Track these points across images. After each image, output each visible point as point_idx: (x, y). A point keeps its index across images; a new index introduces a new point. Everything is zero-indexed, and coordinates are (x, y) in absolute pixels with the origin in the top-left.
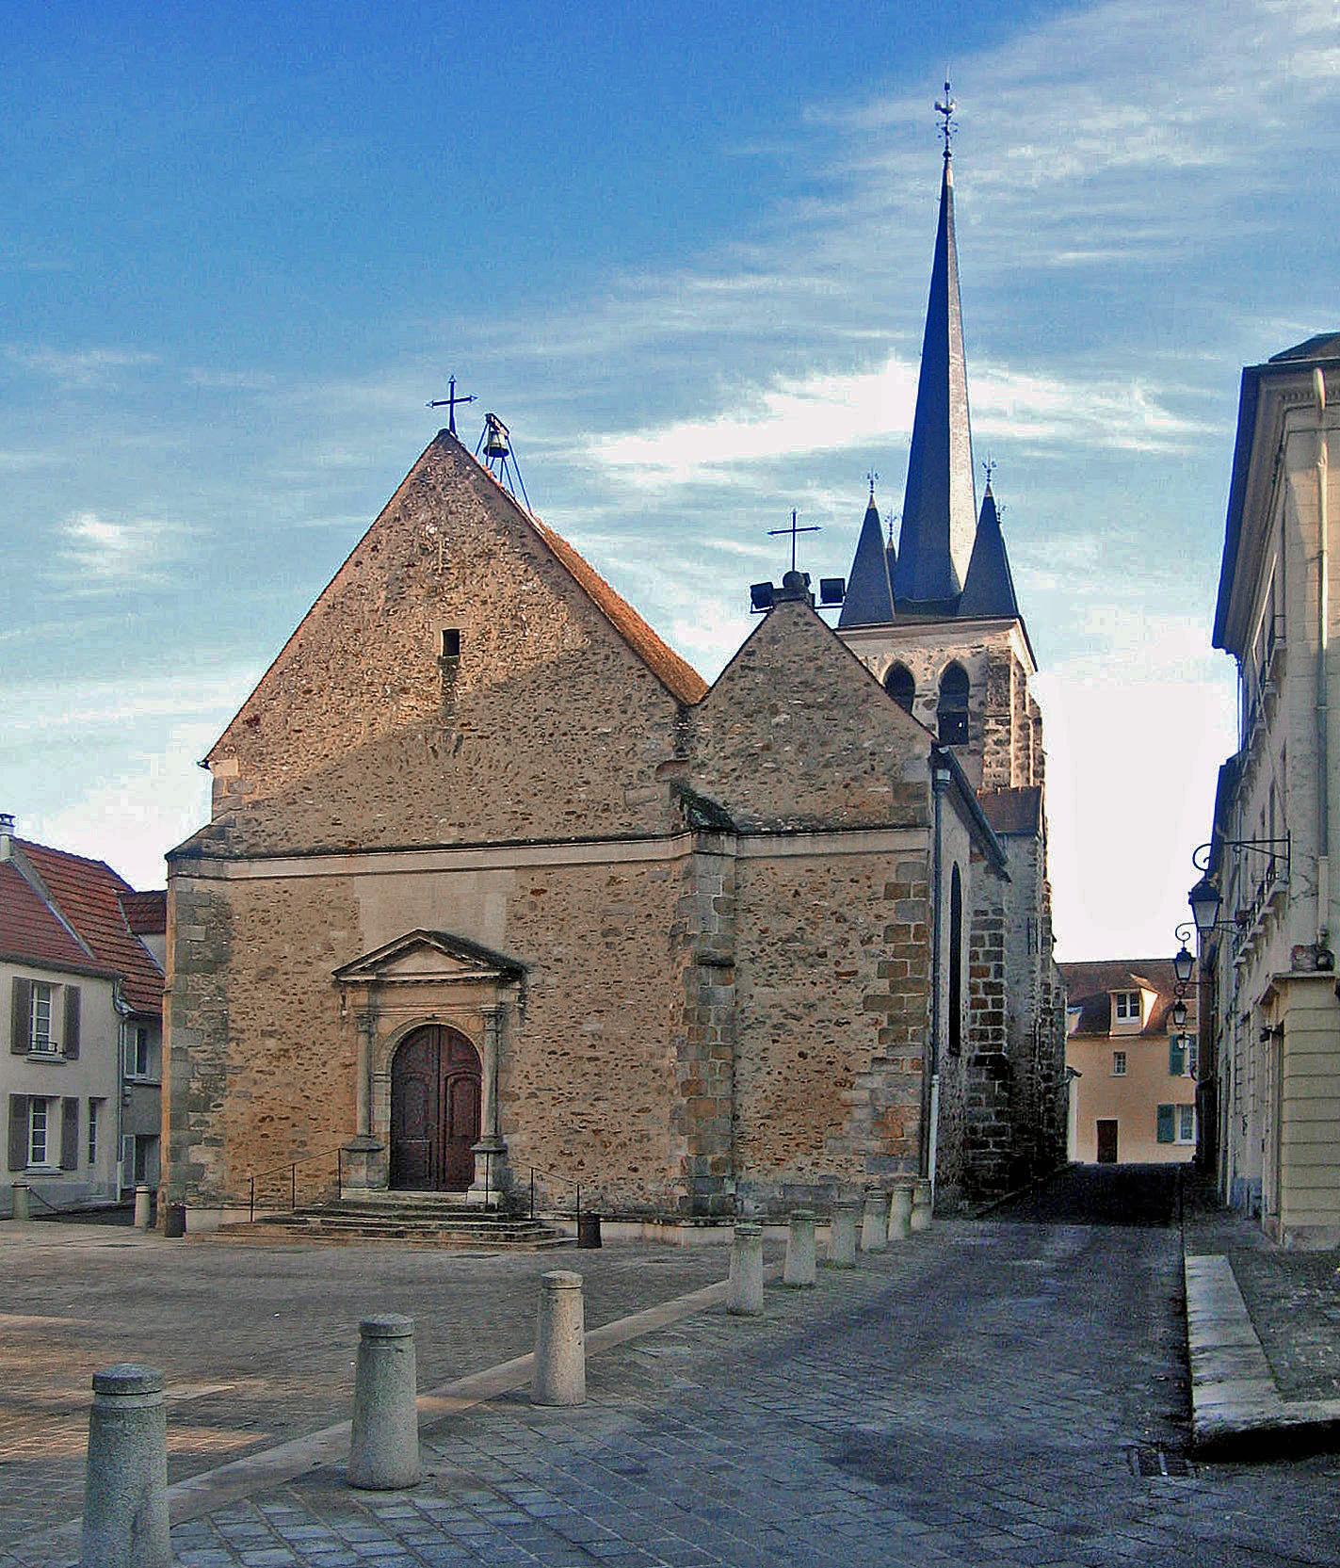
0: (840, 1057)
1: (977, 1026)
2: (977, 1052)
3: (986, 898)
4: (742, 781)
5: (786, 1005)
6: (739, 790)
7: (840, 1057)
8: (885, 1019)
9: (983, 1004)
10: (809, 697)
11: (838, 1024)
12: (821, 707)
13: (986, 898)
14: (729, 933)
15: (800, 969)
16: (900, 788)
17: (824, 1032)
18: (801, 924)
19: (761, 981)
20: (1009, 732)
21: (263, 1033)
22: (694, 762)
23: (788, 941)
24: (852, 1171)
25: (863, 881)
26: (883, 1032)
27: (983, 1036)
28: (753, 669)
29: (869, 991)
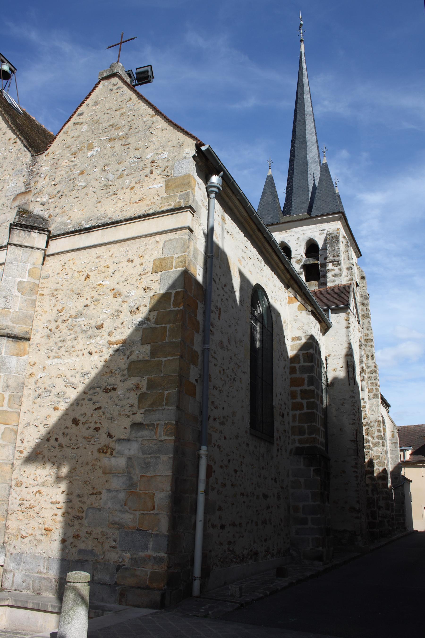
0: (106, 424)
1: (297, 424)
2: (297, 445)
3: (299, 328)
4: (63, 199)
5: (69, 374)
6: (60, 205)
7: (106, 424)
8: (144, 384)
9: (299, 406)
10: (114, 134)
11: (106, 391)
12: (118, 138)
13: (299, 328)
14: (30, 311)
15: (82, 340)
16: (171, 184)
17: (95, 398)
18: (88, 302)
19: (52, 354)
20: (340, 269)
21: (92, 451)
22: (35, 191)
23: (76, 317)
24: (107, 546)
25: (137, 261)
26: (142, 397)
27: (301, 432)
28: (81, 124)
29: (134, 357)
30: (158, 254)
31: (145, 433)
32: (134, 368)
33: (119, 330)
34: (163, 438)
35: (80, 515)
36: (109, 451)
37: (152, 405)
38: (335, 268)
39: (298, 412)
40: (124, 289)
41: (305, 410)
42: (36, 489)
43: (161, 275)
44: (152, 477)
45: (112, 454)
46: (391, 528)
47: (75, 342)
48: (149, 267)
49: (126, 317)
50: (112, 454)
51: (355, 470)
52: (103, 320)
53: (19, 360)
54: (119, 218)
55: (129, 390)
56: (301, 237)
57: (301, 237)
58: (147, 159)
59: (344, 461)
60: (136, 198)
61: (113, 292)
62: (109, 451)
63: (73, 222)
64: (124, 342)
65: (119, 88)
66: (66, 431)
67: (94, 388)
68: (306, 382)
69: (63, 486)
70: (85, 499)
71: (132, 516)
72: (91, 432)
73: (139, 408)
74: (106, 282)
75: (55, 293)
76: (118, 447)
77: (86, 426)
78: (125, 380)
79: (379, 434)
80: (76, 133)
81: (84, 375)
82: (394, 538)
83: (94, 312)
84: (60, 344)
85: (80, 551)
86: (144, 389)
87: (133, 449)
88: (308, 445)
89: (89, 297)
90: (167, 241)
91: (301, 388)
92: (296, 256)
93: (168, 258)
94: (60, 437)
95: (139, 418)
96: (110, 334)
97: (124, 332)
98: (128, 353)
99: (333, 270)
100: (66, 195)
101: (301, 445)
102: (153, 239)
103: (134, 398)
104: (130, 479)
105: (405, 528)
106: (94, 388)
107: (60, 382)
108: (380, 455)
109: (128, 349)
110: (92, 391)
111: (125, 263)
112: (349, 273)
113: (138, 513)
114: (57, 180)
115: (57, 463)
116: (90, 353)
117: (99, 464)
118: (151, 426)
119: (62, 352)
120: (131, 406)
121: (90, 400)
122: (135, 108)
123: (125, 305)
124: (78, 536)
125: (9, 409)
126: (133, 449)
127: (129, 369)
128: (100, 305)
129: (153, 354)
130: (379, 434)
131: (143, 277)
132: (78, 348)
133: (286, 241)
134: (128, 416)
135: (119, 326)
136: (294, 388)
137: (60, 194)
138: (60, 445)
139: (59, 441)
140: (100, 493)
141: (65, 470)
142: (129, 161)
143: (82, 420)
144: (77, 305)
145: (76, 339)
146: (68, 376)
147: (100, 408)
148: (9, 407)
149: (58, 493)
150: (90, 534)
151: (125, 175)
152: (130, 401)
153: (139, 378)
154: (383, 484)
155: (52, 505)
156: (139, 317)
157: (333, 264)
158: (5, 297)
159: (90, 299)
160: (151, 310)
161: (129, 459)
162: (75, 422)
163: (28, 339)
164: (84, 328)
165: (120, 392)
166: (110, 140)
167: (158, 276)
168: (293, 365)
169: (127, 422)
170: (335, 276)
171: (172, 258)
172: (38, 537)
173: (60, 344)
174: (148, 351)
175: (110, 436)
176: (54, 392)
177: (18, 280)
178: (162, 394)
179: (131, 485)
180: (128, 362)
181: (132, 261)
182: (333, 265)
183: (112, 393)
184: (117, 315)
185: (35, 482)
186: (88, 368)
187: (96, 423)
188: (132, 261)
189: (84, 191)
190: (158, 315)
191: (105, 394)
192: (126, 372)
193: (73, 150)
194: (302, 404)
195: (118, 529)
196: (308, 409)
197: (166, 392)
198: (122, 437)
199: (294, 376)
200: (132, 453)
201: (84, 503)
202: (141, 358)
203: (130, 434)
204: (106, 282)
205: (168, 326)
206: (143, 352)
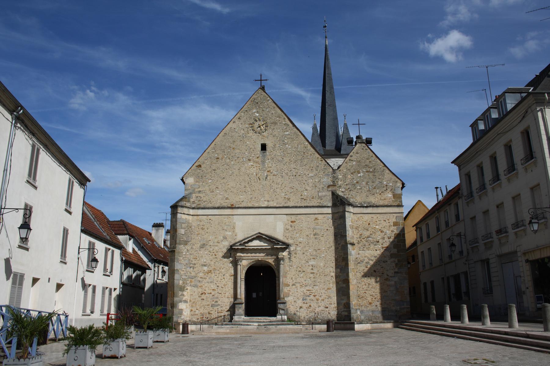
5: (369, 256)
11: (384, 262)
12: (371, 172)
19: (361, 249)
26: (396, 264)
29: (392, 252)
30: (394, 220)
32: (392, 256)
40: (385, 230)
48: (392, 224)
49: (386, 239)
54: (378, 205)
60: (382, 198)
64: (387, 247)
69: (378, 284)
74: (377, 227)
81: (375, 257)
87: (396, 279)
95: (396, 270)
97: (386, 245)
102: (392, 215)
103: (394, 264)
107: (366, 258)
111: (382, 222)
114: (347, 183)
115: (376, 277)
119: (365, 249)
141: (378, 279)
142: (377, 182)
144: (367, 233)
149: (378, 286)
156: (391, 240)
160: (395, 238)
161: (395, 282)
162: (375, 271)
166: (367, 172)
167: (396, 227)
169: (393, 271)
175: (388, 275)
176: (365, 262)
184: (383, 238)
186: (376, 255)
193: (352, 172)
204: (377, 227)
206: (395, 251)
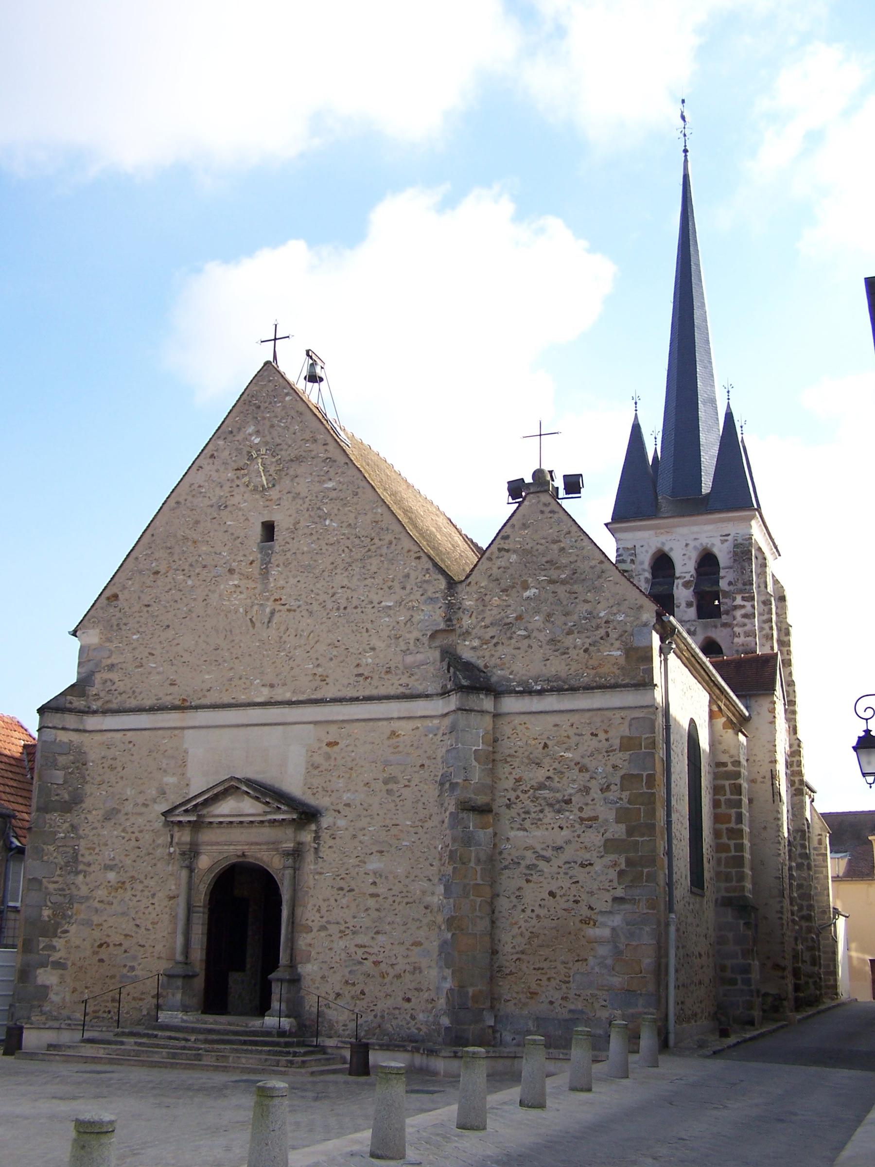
1: (722, 869)
4: (500, 647)
5: (538, 848)
6: (497, 655)
11: (582, 865)
15: (549, 814)
17: (571, 873)
18: (550, 774)
25: (602, 736)
26: (621, 873)
28: (508, 551)
29: (609, 835)
31: (627, 906)
33: (589, 807)
34: (645, 911)
35: (567, 979)
36: (592, 923)
37: (632, 881)
38: (745, 603)
39: (724, 855)
41: (733, 853)
42: (515, 957)
43: (631, 755)
44: (637, 946)
45: (595, 925)
46: (818, 992)
47: (541, 815)
48: (616, 743)
50: (595, 925)
51: (780, 915)
52: (570, 795)
53: (485, 833)
55: (607, 867)
56: (692, 544)
57: (692, 544)
58: (600, 618)
59: (766, 904)
61: (579, 766)
62: (592, 923)
63: (517, 680)
65: (552, 512)
66: (542, 903)
67: (569, 863)
68: (733, 819)
70: (570, 965)
71: (620, 979)
72: (570, 904)
73: (619, 884)
75: (509, 759)
76: (601, 919)
77: (565, 898)
78: (602, 857)
79: (803, 851)
80: (501, 562)
82: (822, 1007)
83: (558, 785)
84: (523, 816)
85: (571, 1011)
86: (623, 866)
88: (736, 894)
89: (551, 769)
90: (634, 719)
91: (727, 826)
92: (683, 575)
93: (636, 737)
94: (536, 909)
95: (620, 892)
96: (581, 809)
98: (602, 831)
99: (743, 607)
100: (503, 644)
101: (729, 895)
103: (613, 874)
104: (616, 947)
105: (837, 994)
106: (569, 863)
108: (804, 882)
109: (602, 827)
110: (568, 865)
112: (766, 610)
113: (626, 977)
116: (561, 828)
117: (582, 933)
118: (633, 901)
119: (527, 824)
120: (611, 881)
121: (566, 874)
122: (577, 544)
123: (593, 781)
124: (567, 997)
125: (481, 882)
126: (617, 920)
127: (605, 846)
128: (565, 779)
129: (630, 832)
130: (803, 851)
131: (611, 754)
132: (545, 821)
133: (666, 549)
134: (608, 891)
135: (590, 802)
136: (718, 826)
137: (495, 641)
138: (538, 916)
139: (536, 912)
140: (586, 960)
143: (559, 893)
145: (542, 811)
146: (539, 850)
147: (578, 882)
148: (483, 880)
150: (579, 996)
151: (576, 632)
152: (610, 877)
153: (617, 856)
154: (807, 926)
155: (534, 972)
157: (743, 597)
158: (465, 768)
159: (552, 771)
161: (613, 929)
163: (490, 811)
164: (550, 801)
165: (597, 867)
166: (552, 582)
168: (717, 797)
169: (608, 897)
170: (745, 616)
171: (640, 738)
172: (523, 1000)
173: (523, 816)
174: (624, 830)
177: (474, 748)
178: (642, 872)
179: (618, 953)
180: (603, 840)
181: (596, 735)
182: (743, 599)
183: (588, 868)
185: (514, 951)
187: (575, 896)
188: (596, 735)
189: (526, 642)
190: (630, 794)
191: (582, 870)
192: (602, 849)
193: (503, 586)
194: (729, 846)
195: (607, 991)
196: (736, 852)
197: (645, 870)
198: (604, 910)
199: (719, 811)
200: (616, 924)
201: (570, 969)
202: (616, 836)
203: (612, 907)
205: (642, 807)
